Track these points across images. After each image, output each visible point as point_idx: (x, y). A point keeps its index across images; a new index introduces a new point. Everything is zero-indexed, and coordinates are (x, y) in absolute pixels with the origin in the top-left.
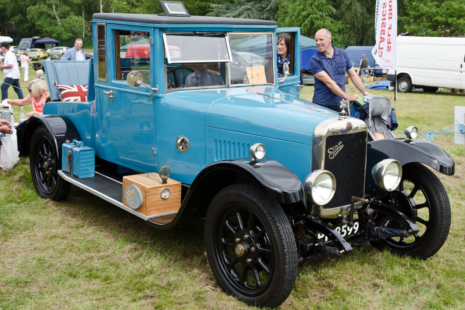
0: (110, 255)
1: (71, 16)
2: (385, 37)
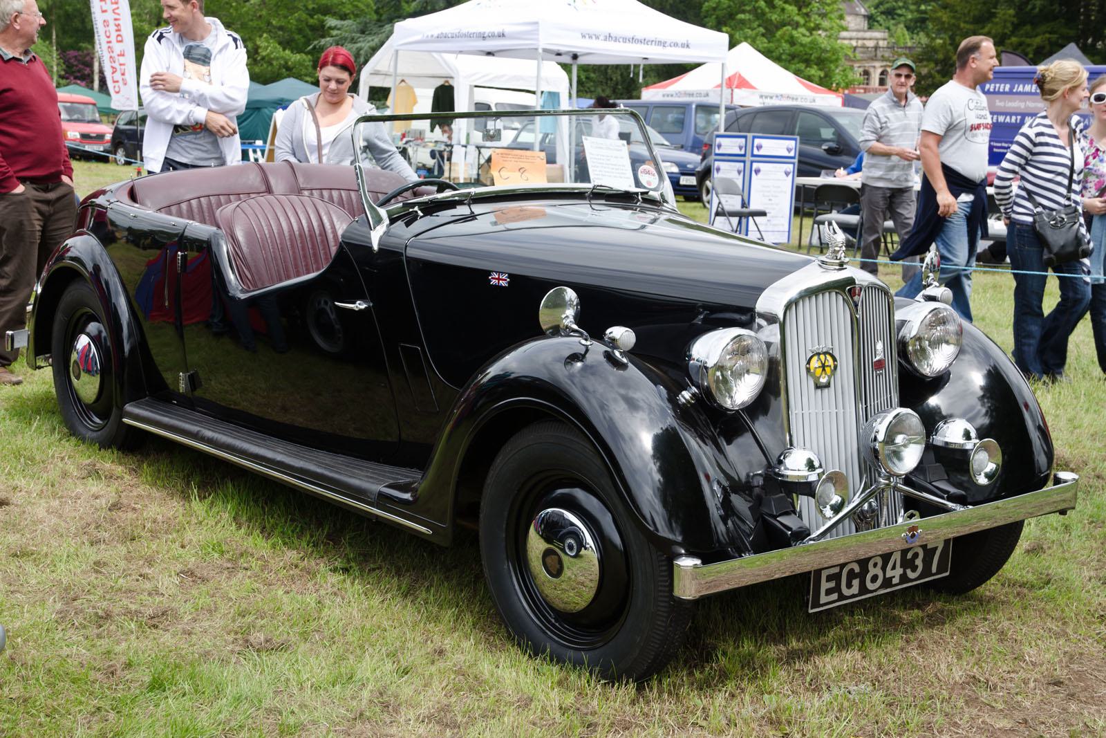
0: (437, 657)
2: (116, 65)
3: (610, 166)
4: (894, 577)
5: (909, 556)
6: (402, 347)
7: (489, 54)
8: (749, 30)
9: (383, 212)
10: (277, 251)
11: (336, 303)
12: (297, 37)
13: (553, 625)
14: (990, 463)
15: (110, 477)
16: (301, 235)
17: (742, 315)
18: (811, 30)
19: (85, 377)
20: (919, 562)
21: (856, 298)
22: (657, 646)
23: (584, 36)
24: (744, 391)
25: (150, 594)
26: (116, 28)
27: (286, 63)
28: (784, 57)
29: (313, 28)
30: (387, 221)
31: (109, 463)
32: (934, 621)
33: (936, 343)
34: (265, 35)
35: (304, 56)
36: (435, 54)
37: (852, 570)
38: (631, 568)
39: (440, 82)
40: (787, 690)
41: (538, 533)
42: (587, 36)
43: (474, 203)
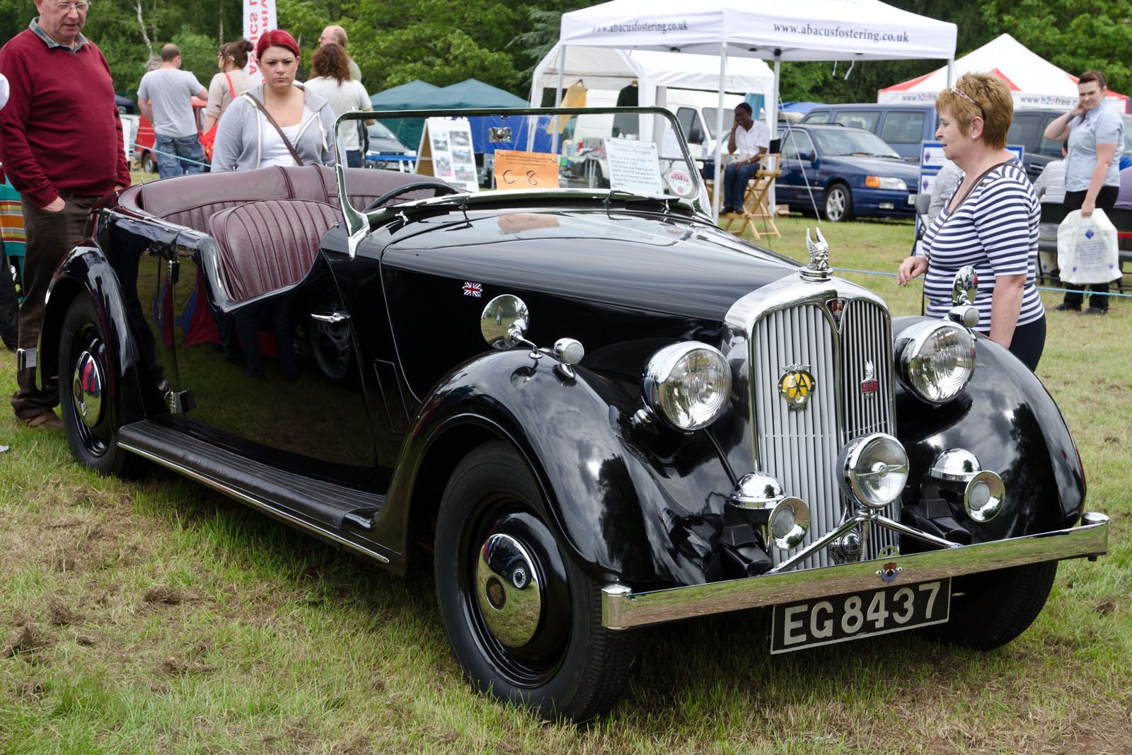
1: (183, 36)
3: (635, 170)
4: (877, 620)
5: (896, 597)
6: (377, 362)
7: (674, 49)
8: (1036, 19)
9: (364, 217)
10: (275, 260)
11: (313, 315)
12: (496, 31)
13: (504, 662)
14: (991, 498)
15: (101, 504)
16: (303, 245)
17: (713, 331)
18: (1115, 18)
19: (88, 399)
20: (909, 605)
21: (837, 313)
22: (595, 683)
23: (777, 28)
24: (699, 413)
25: (101, 623)
26: (263, 22)
27: (483, 62)
28: (1080, 51)
29: (515, 23)
30: (368, 227)
31: (106, 489)
32: (944, 674)
33: (948, 365)
34: (458, 31)
35: (503, 55)
36: (617, 51)
37: (823, 611)
38: (568, 599)
39: (626, 83)
40: (744, 738)
41: (487, 562)
42: (790, 29)
43: (468, 209)
